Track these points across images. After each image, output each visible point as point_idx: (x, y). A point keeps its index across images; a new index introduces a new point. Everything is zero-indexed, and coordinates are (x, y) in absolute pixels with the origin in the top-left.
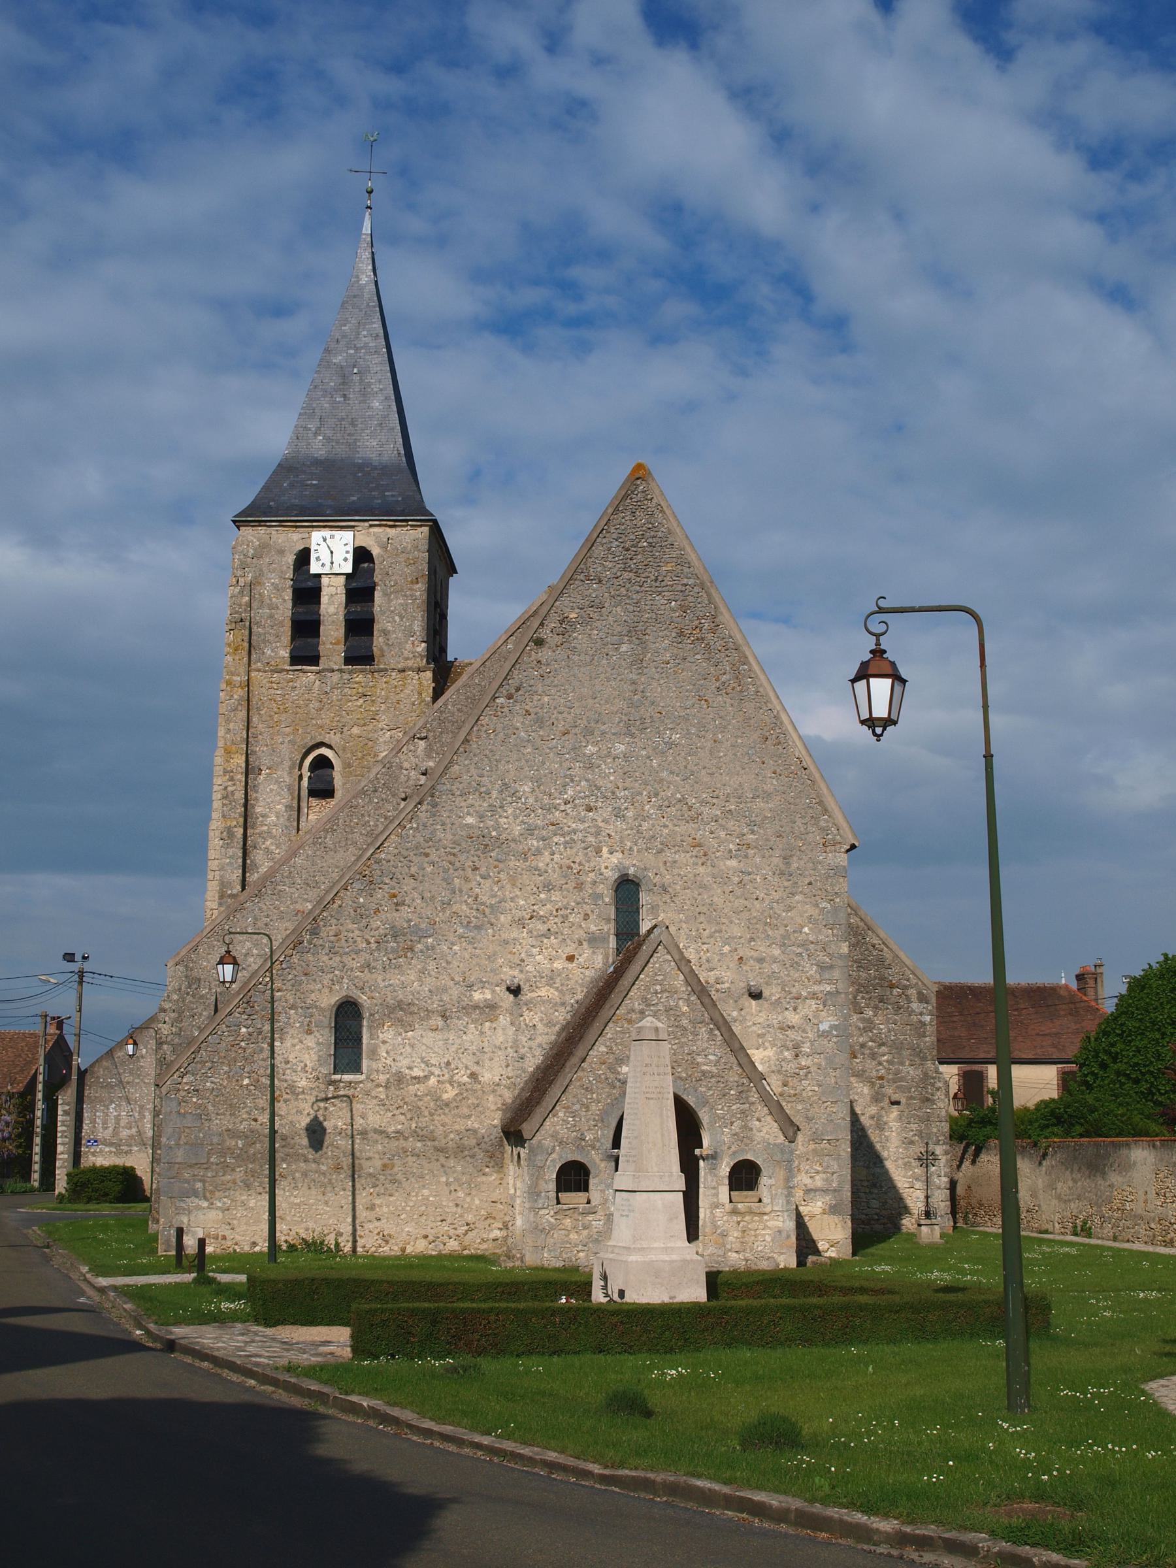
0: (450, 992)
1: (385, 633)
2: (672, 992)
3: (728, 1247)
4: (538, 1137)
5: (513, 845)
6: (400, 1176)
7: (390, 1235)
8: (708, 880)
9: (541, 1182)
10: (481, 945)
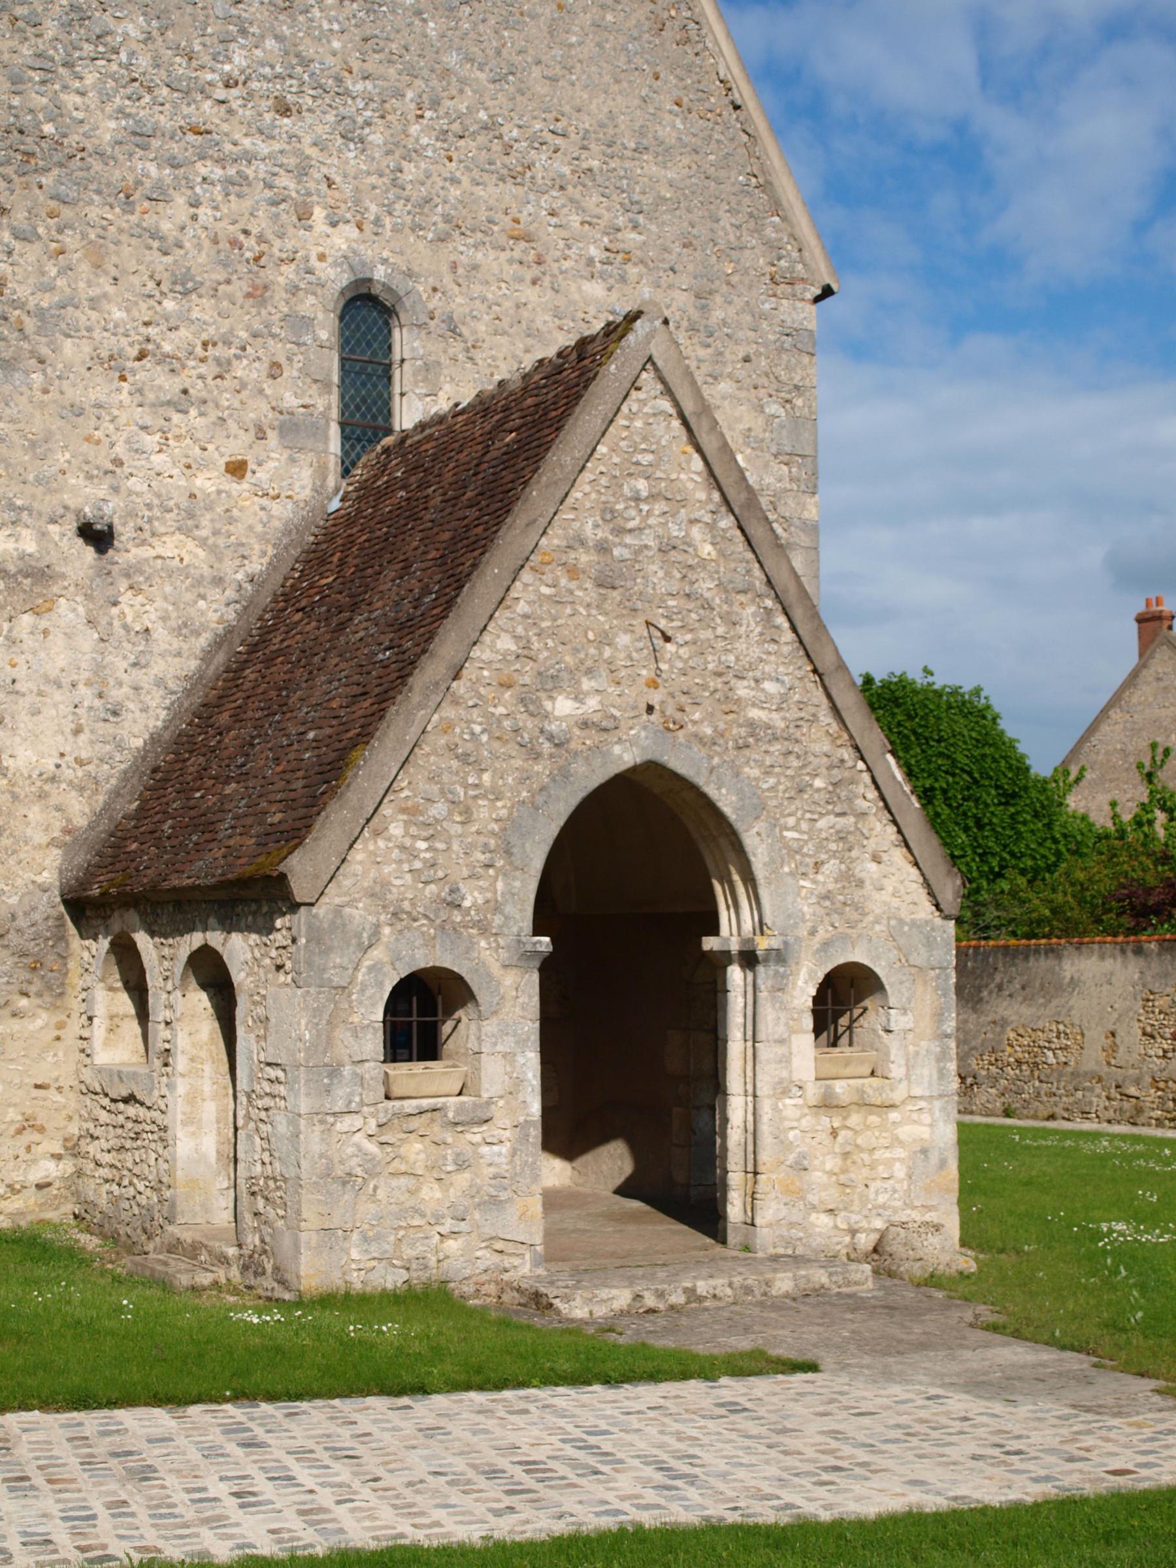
2: (677, 501)
4: (333, 898)
5: (97, 166)
9: (342, 1035)
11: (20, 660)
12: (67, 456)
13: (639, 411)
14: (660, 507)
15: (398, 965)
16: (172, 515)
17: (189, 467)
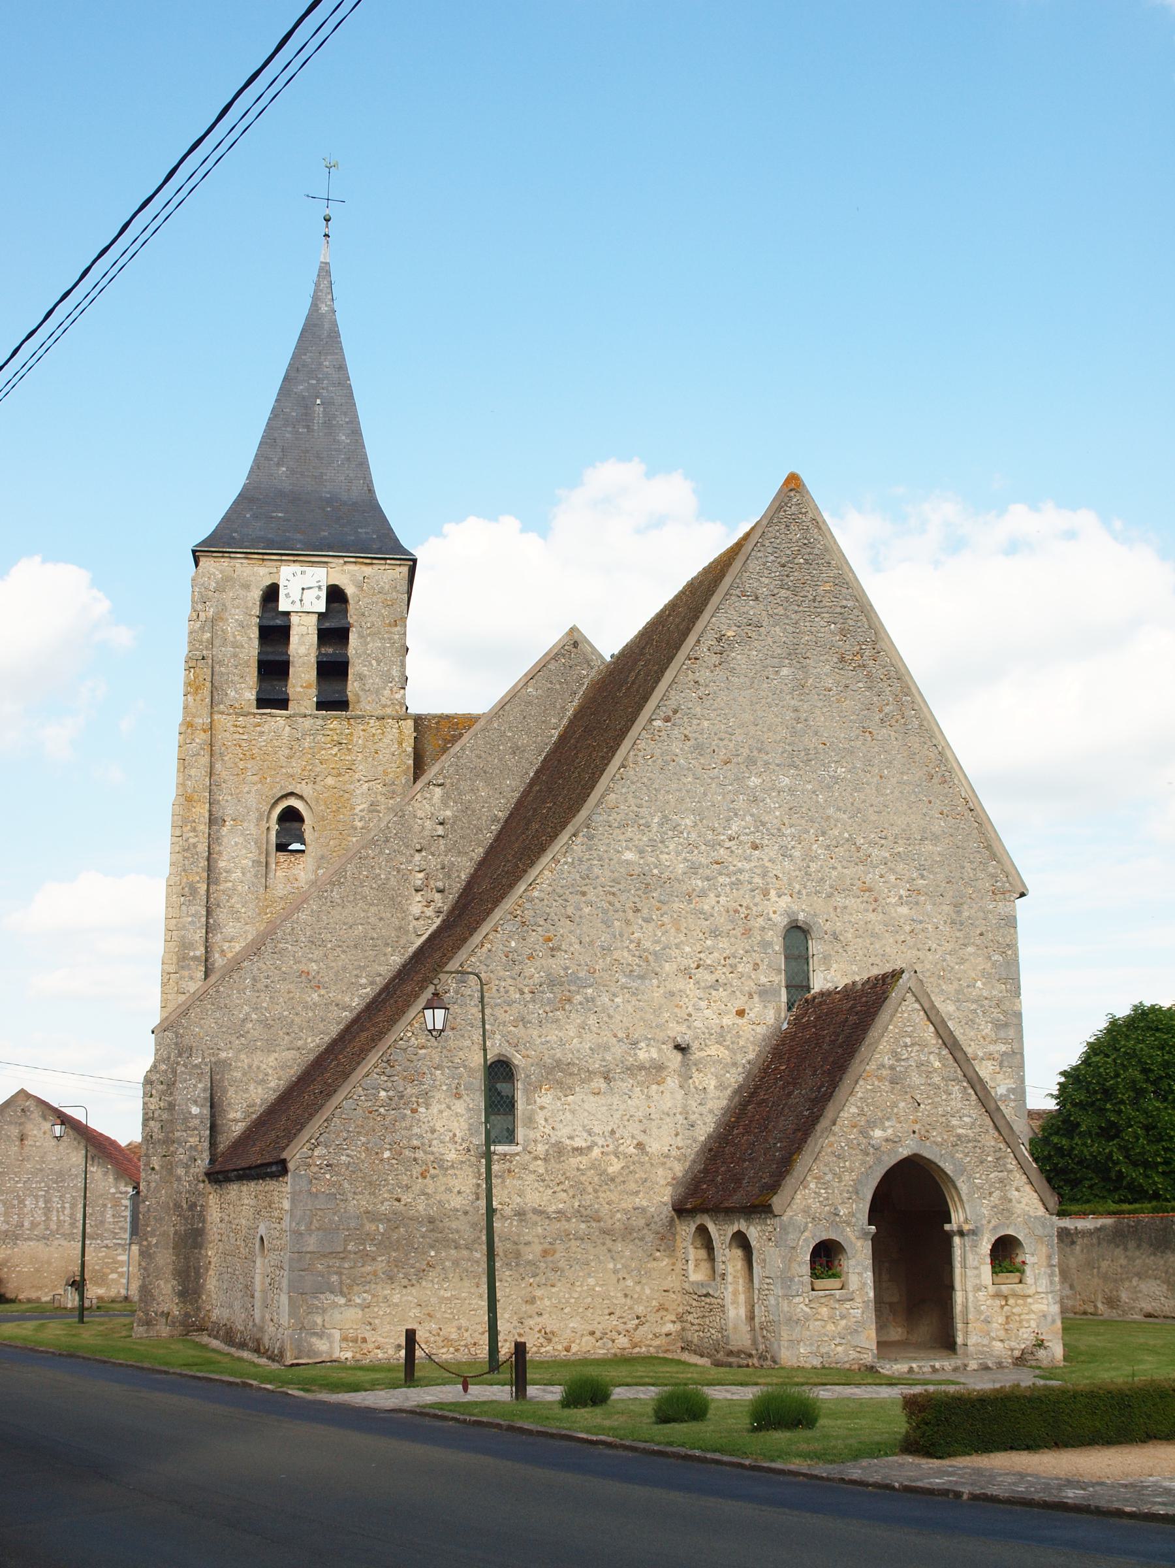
0: (613, 1050)
1: (361, 677)
2: (923, 1045)
4: (789, 1213)
6: (562, 1264)
7: (553, 1333)
8: (879, 928)
9: (794, 1265)
10: (645, 997)
11: (652, 1105)
14: (916, 1048)
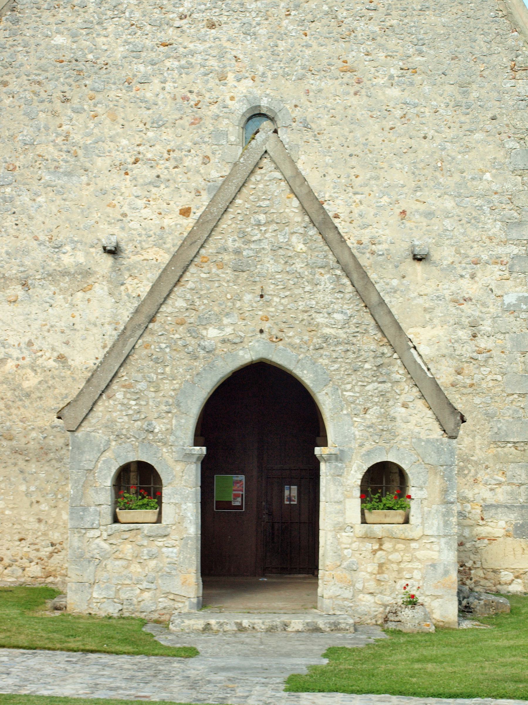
3: (359, 586)
5: (114, 71)
9: (91, 492)
10: (72, 196)
11: (77, 314)
12: (99, 214)
13: (262, 179)
15: (118, 459)
16: (151, 239)
17: (160, 214)
